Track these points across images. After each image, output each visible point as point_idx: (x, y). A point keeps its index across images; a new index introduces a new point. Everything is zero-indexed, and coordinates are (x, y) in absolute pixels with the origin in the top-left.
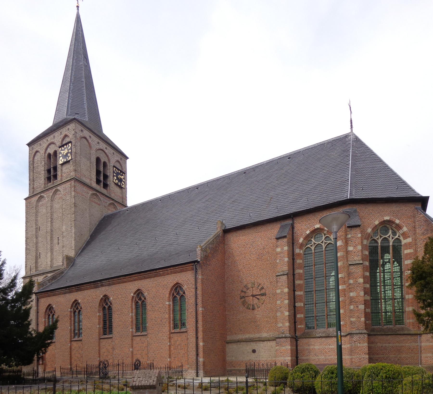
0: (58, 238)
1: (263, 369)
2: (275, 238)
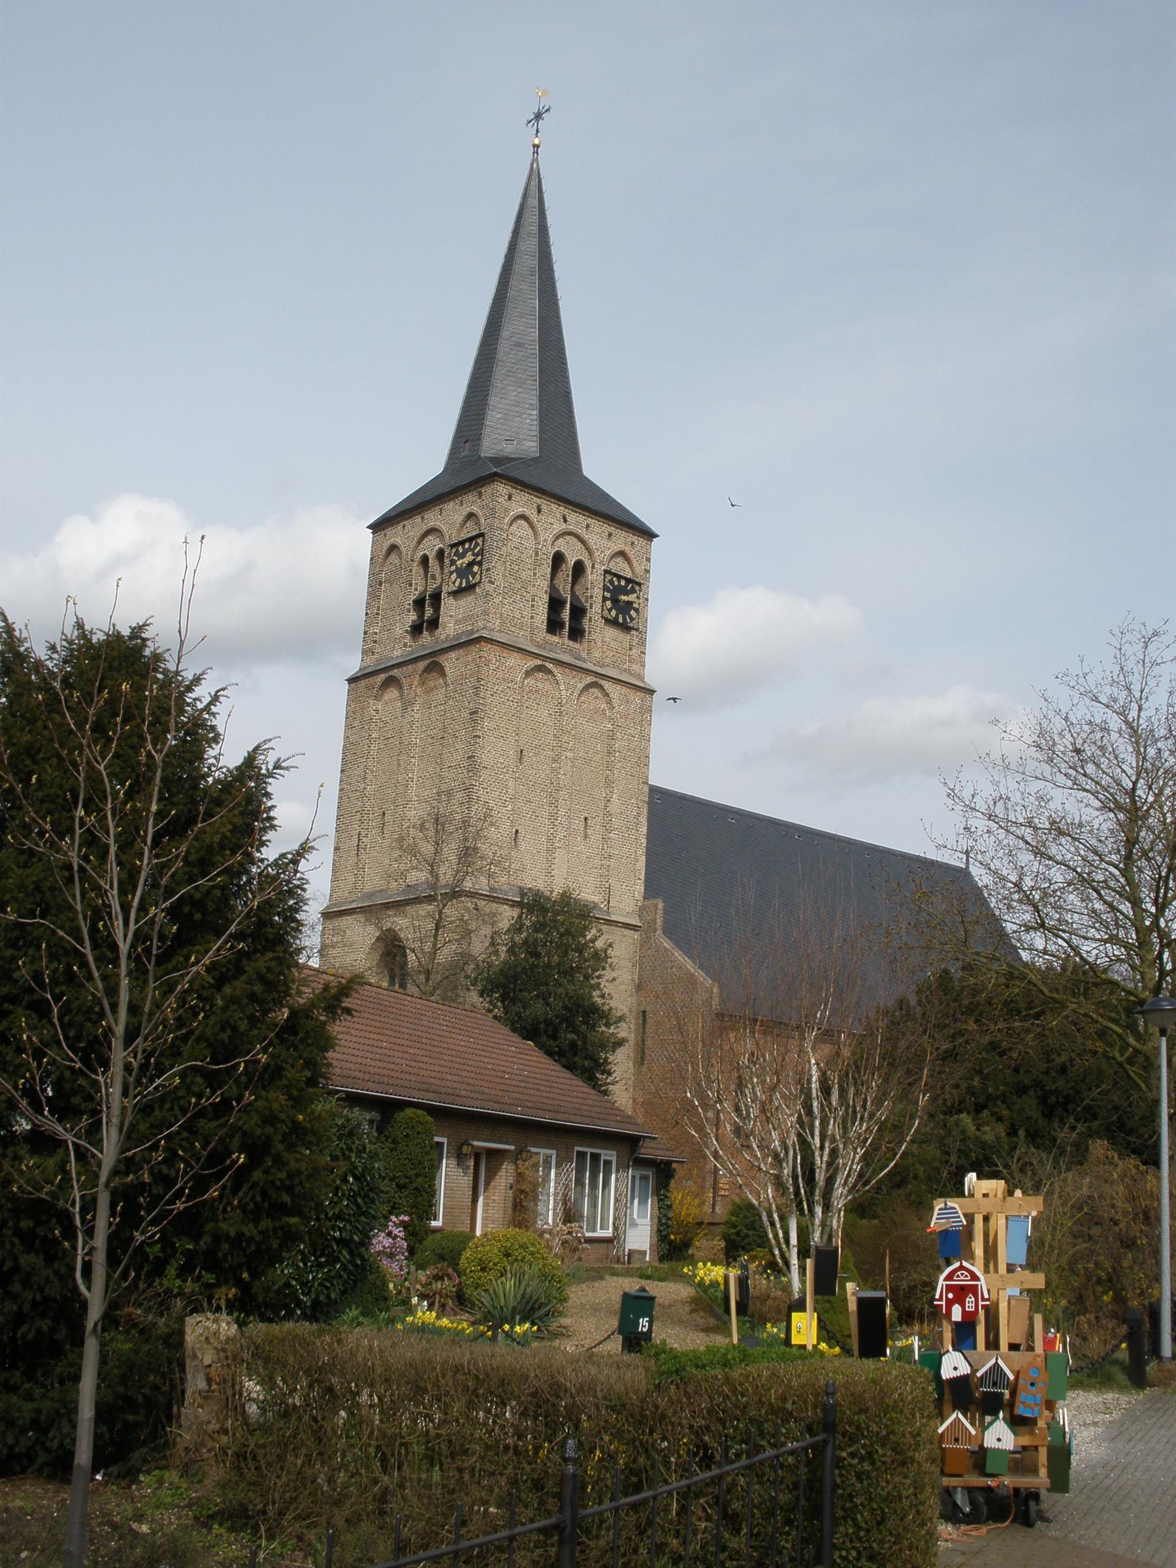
0: (586, 819)
1: (922, 1322)
2: (353, 1016)
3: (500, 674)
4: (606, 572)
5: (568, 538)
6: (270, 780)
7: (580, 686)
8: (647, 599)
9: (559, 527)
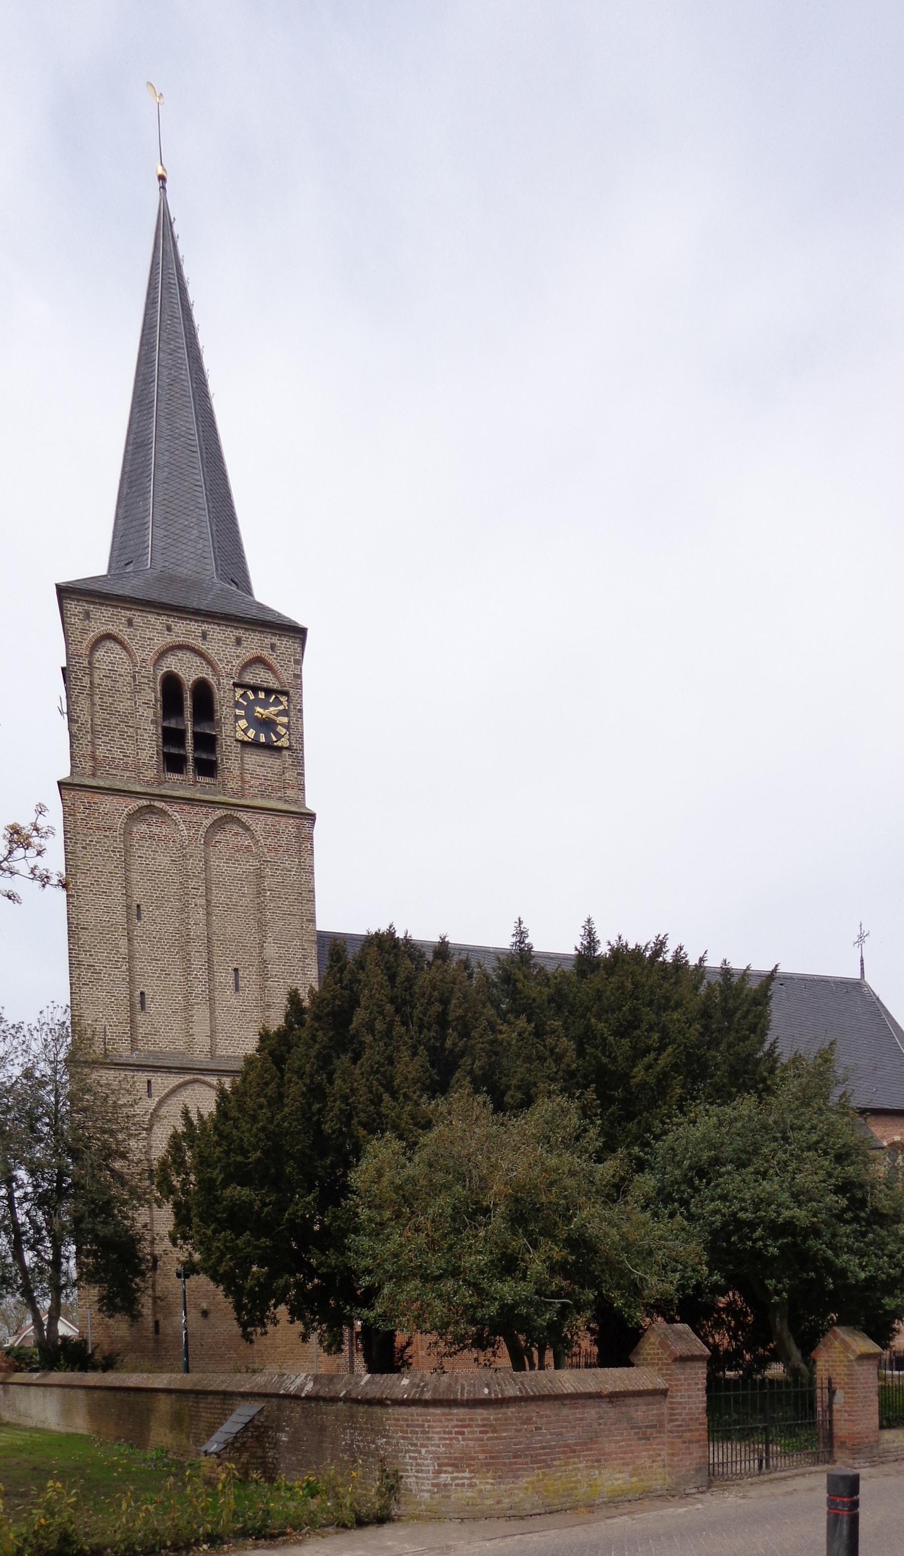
0: (236, 970)
3: (93, 823)
4: (235, 685)
5: (180, 654)
6: (446, 940)
7: (207, 822)
8: (300, 711)
9: (161, 641)
